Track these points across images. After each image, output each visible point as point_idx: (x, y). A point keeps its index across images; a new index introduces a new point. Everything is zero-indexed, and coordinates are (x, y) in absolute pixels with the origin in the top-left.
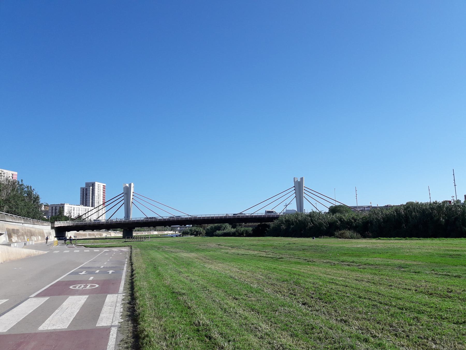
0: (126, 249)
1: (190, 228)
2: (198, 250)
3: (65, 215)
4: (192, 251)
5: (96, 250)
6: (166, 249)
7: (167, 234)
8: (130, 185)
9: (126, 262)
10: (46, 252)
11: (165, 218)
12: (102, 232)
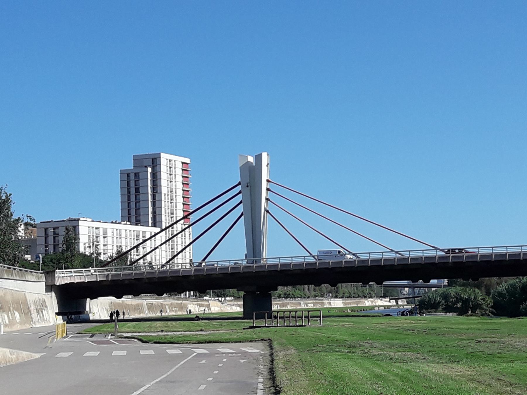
0: (254, 349)
1: (441, 290)
2: (472, 356)
3: (82, 250)
4: (454, 360)
5: (173, 350)
6: (375, 352)
7: (372, 308)
8: (258, 158)
9: (261, 386)
10: (38, 356)
11: (363, 257)
12: (185, 299)
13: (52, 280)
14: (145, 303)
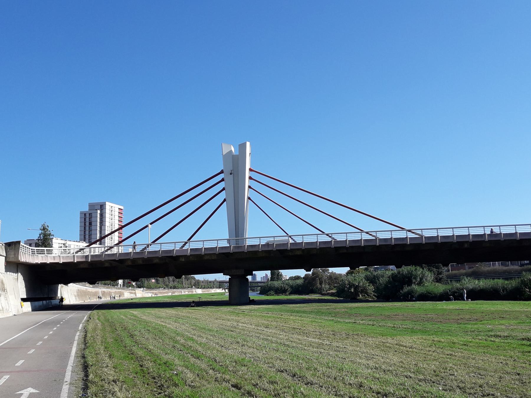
8: (243, 147)
13: (15, 254)
14: (100, 291)
